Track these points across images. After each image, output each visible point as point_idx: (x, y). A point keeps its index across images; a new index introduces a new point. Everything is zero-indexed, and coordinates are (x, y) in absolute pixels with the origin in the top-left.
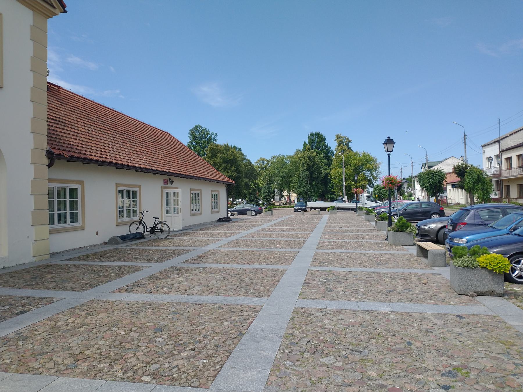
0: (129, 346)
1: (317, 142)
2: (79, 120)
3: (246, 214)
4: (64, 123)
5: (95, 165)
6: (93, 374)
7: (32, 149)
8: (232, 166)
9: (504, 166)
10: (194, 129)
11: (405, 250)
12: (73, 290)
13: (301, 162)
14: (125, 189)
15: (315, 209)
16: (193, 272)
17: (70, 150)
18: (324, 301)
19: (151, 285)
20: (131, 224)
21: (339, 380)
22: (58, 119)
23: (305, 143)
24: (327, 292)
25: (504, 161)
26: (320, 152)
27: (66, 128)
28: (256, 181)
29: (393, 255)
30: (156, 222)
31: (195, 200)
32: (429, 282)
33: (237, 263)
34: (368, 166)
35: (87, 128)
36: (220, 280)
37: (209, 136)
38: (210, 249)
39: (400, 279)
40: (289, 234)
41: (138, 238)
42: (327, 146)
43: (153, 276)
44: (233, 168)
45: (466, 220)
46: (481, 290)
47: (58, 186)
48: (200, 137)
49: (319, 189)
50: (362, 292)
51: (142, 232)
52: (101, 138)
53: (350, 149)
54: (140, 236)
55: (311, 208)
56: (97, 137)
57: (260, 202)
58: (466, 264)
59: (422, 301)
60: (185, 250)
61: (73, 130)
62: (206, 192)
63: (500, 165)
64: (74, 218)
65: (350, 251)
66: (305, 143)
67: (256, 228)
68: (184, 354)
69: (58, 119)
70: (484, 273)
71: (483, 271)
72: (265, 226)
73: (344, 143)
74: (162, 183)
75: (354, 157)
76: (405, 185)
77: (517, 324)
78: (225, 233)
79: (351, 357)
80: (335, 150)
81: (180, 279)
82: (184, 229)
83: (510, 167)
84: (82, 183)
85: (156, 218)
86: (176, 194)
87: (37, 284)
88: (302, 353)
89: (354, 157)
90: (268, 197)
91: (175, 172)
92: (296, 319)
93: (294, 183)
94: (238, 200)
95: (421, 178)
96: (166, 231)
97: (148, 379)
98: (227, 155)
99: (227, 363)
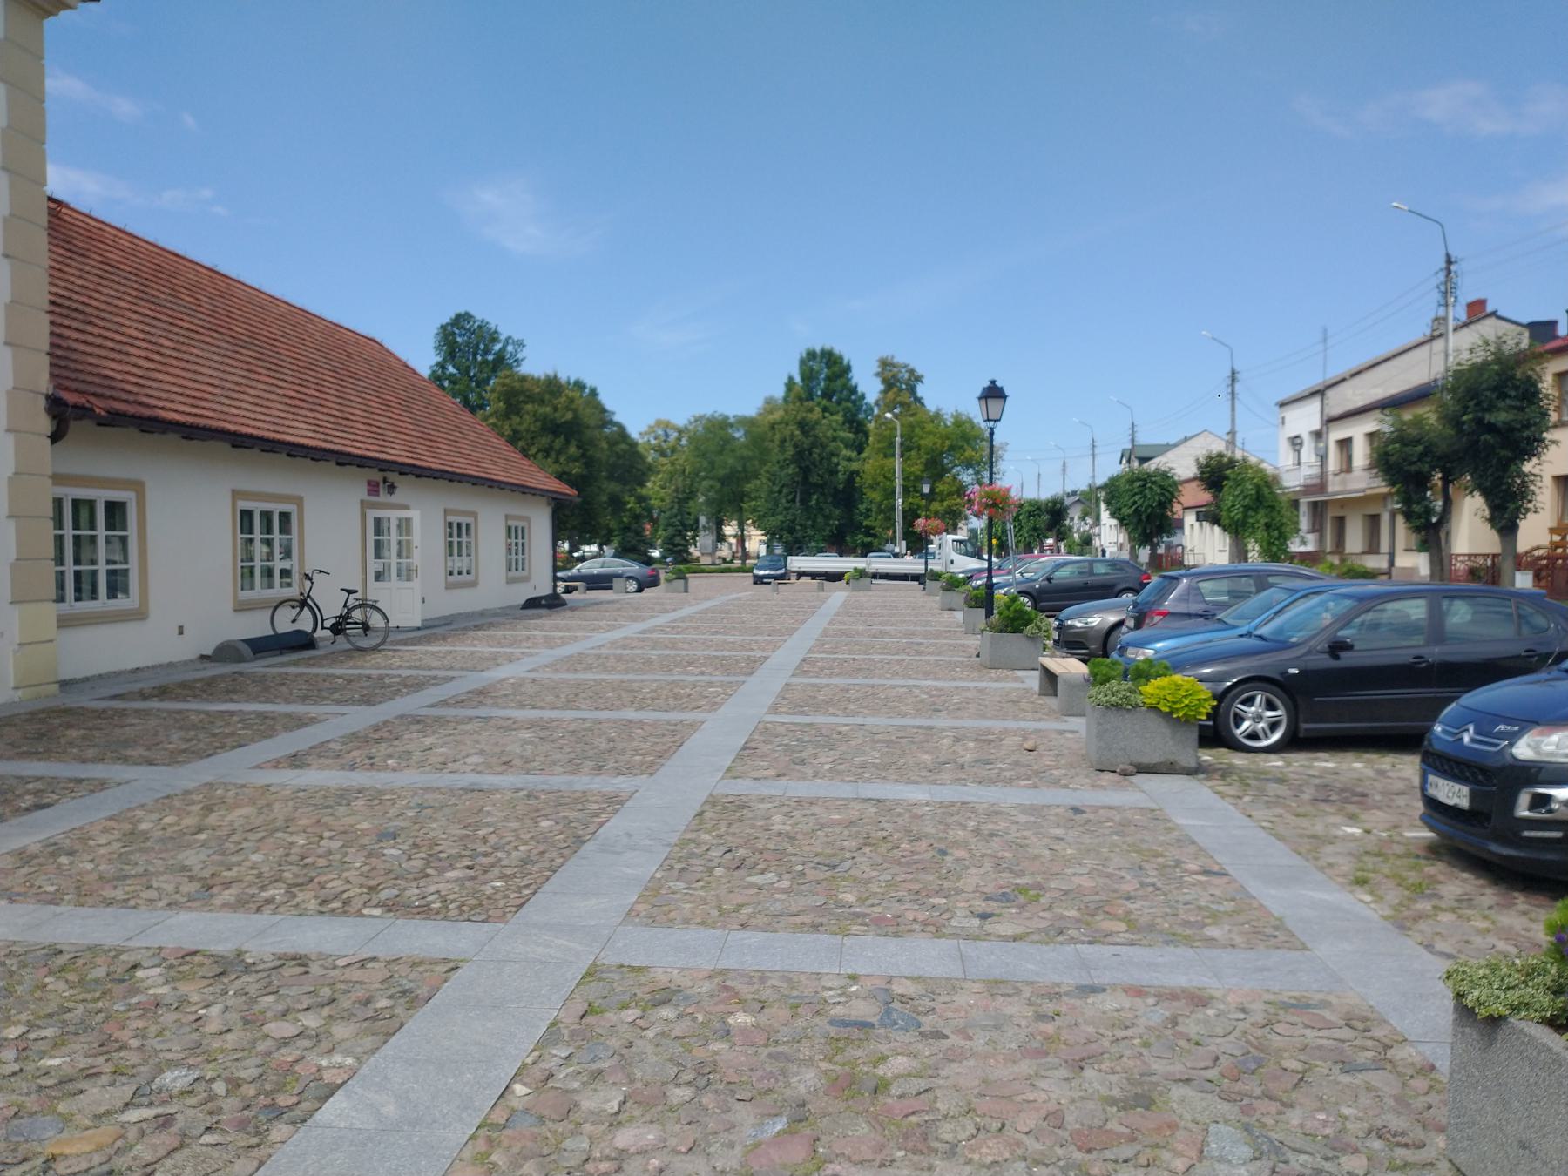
0: (322, 862)
1: (825, 375)
2: (122, 304)
3: (610, 588)
4: (83, 312)
5: (133, 432)
6: (254, 906)
7: (8, 393)
8: (568, 442)
9: (1333, 463)
10: (453, 325)
11: (1016, 679)
12: (151, 763)
13: (777, 437)
14: (257, 507)
15: (813, 575)
16: (461, 727)
17: (108, 392)
18: (783, 782)
19: (355, 753)
20: (276, 608)
21: (778, 907)
22: (68, 303)
23: (791, 379)
24: (794, 764)
25: (1333, 451)
26: (832, 406)
27: (90, 328)
28: (644, 492)
29: (980, 691)
30: (351, 603)
31: (459, 543)
32: (1042, 748)
33: (578, 708)
34: (969, 452)
35: (147, 328)
36: (531, 743)
37: (497, 347)
38: (503, 675)
39: (975, 740)
40: (725, 642)
41: (293, 649)
42: (854, 390)
43: (354, 736)
44: (573, 450)
45: (1169, 604)
46: (1145, 760)
47: (71, 493)
48: (471, 352)
49: (827, 517)
50: (875, 766)
51: (309, 629)
52: (186, 357)
53: (919, 400)
54: (301, 642)
55: (800, 574)
56: (176, 354)
57: (656, 554)
58: (1113, 699)
59: (1009, 782)
60: (435, 678)
61: (110, 334)
62: (490, 522)
63: (1323, 459)
64: (117, 584)
65: (876, 681)
66: (791, 379)
67: (634, 624)
68: (451, 875)
69: (68, 303)
70: (1155, 723)
71: (1152, 715)
72: (662, 620)
73: (900, 384)
74: (361, 492)
75: (930, 427)
76: (1075, 513)
77: (1191, 822)
78: (546, 637)
79: (811, 874)
80: (877, 404)
81: (428, 741)
82: (427, 625)
83: (1347, 467)
84: (138, 487)
85: (350, 592)
86: (405, 526)
87: (48, 751)
88: (711, 870)
89: (930, 427)
90: (678, 540)
91: (400, 460)
92: (708, 815)
93: (755, 499)
94: (587, 548)
95: (1113, 492)
96: (377, 630)
97: (377, 912)
98: (555, 409)
99: (546, 887)
